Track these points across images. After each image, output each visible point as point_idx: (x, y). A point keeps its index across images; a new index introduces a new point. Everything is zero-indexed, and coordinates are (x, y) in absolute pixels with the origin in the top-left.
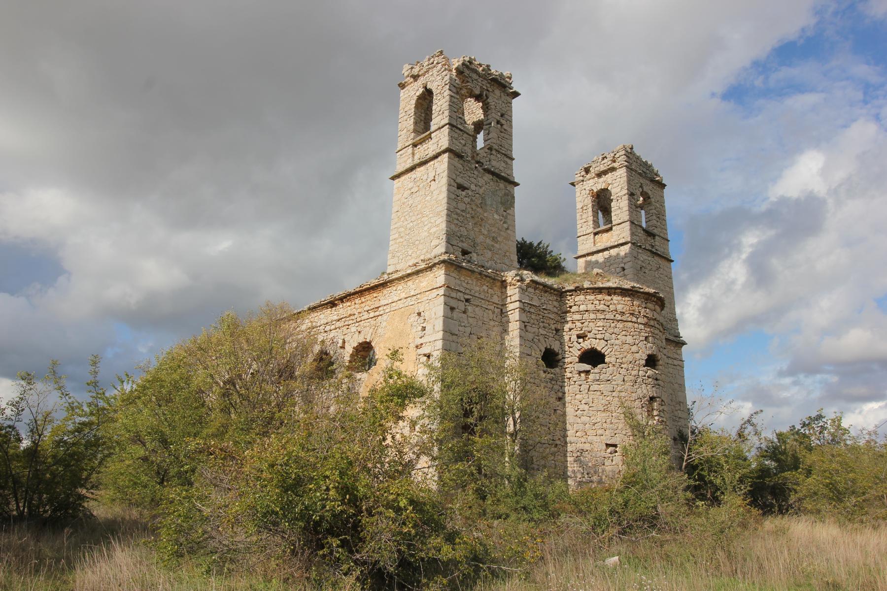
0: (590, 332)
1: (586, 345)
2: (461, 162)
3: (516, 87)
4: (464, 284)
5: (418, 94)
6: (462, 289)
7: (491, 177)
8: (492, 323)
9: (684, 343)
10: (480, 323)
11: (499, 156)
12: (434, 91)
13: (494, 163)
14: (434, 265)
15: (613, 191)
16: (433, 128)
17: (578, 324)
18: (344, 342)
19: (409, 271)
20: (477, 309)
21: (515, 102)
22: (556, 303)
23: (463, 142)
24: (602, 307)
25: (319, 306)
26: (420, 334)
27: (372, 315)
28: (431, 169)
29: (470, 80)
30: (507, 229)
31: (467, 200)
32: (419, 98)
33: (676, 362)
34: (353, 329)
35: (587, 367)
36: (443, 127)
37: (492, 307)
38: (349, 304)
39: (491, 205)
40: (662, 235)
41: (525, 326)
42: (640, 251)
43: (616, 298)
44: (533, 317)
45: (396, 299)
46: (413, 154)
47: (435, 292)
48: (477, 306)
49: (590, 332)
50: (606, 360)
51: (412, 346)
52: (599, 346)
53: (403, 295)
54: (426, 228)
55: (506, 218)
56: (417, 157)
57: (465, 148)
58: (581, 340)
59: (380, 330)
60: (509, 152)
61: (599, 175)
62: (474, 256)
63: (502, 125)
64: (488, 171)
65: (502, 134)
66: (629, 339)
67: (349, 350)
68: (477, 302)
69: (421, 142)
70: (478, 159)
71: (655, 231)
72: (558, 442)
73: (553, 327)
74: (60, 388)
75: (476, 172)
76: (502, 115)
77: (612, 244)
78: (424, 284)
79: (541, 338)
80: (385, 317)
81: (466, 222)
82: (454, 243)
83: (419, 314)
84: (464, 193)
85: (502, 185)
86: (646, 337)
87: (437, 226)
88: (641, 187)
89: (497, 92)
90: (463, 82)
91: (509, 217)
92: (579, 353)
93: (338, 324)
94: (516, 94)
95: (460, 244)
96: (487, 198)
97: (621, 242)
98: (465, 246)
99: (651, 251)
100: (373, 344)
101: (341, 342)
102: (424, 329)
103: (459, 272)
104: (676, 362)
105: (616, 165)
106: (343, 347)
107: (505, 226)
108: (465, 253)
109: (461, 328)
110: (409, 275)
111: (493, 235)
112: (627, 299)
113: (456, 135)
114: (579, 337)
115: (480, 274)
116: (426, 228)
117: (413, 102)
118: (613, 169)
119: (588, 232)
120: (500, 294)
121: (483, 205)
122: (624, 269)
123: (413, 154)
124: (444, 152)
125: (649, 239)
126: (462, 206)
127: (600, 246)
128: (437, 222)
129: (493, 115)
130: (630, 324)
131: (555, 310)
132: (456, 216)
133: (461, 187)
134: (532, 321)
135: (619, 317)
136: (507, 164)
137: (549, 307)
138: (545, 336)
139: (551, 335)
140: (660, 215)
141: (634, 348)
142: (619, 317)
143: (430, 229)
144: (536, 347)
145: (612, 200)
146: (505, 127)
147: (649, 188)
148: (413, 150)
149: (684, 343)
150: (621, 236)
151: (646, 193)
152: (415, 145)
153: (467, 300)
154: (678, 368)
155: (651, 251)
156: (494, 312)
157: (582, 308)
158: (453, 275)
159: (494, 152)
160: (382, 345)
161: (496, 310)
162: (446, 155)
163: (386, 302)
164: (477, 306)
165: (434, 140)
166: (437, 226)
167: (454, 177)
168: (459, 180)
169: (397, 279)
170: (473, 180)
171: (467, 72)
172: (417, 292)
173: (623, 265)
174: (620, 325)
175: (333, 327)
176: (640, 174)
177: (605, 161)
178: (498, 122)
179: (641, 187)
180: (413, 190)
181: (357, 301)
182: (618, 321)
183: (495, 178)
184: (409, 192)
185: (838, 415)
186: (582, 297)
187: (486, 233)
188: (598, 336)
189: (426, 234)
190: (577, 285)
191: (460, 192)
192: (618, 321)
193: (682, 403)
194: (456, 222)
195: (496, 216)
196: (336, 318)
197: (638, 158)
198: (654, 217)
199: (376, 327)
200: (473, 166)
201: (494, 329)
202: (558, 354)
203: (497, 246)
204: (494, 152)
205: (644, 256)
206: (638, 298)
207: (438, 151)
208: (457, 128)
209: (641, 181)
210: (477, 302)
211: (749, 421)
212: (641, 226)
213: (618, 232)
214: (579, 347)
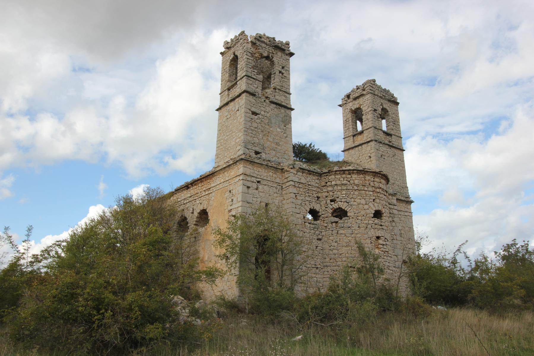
0: (338, 198)
1: (336, 206)
2: (254, 98)
3: (292, 49)
4: (257, 172)
5: (231, 58)
6: (255, 175)
7: (275, 106)
8: (275, 195)
9: (412, 202)
10: (268, 195)
11: (281, 93)
12: (238, 56)
13: (277, 97)
14: (237, 161)
15: (363, 109)
16: (238, 78)
17: (331, 193)
18: (193, 210)
19: (224, 166)
20: (265, 187)
21: (292, 59)
22: (317, 181)
23: (256, 86)
24: (345, 182)
25: (181, 188)
26: (231, 203)
27: (207, 193)
28: (237, 103)
29: (260, 48)
30: (286, 137)
31: (258, 121)
32: (231, 61)
33: (406, 214)
34: (198, 202)
35: (337, 219)
36: (243, 77)
37: (275, 185)
38: (195, 187)
39: (275, 123)
40: (396, 134)
41: (296, 196)
42: (381, 145)
43: (354, 176)
44: (301, 190)
45: (219, 183)
46: (228, 95)
47: (238, 178)
48: (265, 185)
49: (338, 198)
50: (348, 214)
51: (227, 210)
52: (344, 206)
53: (222, 181)
54: (234, 140)
55: (285, 130)
56: (230, 96)
57: (257, 89)
58: (333, 203)
59: (211, 202)
60: (287, 90)
61: (355, 99)
62: (263, 155)
63: (283, 74)
64: (272, 102)
65: (283, 79)
66: (363, 201)
67: (196, 214)
68: (265, 183)
69: (232, 86)
70: (267, 95)
71: (392, 132)
72: (319, 266)
73: (315, 196)
74: (11, 242)
75: (264, 104)
76: (283, 68)
77: (363, 142)
78: (232, 173)
79: (307, 203)
80: (213, 194)
81: (258, 134)
82: (250, 147)
83: (230, 191)
84: (256, 117)
85: (283, 110)
86: (374, 200)
87: (240, 138)
88: (382, 105)
89: (279, 54)
90: (256, 49)
91: (287, 129)
92: (331, 211)
93: (190, 199)
94: (292, 54)
95: (253, 148)
96: (272, 119)
97: (368, 140)
98: (257, 149)
99: (389, 145)
100: (207, 211)
101: (191, 209)
102: (232, 200)
103: (253, 165)
104: (406, 214)
105: (364, 92)
106: (193, 213)
107: (285, 135)
108: (257, 153)
109: (254, 199)
110: (225, 168)
111: (276, 141)
112: (361, 176)
113: (251, 82)
114: (331, 201)
115: (267, 165)
116: (234, 140)
117: (228, 63)
118: (362, 95)
119: (349, 135)
120: (281, 177)
121: (269, 123)
122: (370, 157)
123: (228, 95)
124: (243, 92)
125: (388, 137)
126: (255, 125)
127: (357, 143)
128: (240, 136)
129: (277, 68)
130: (364, 191)
131: (317, 185)
132: (251, 131)
133: (254, 113)
134: (300, 193)
135: (356, 188)
136: (286, 97)
137: (312, 183)
138: (310, 202)
139: (314, 200)
140: (395, 122)
141: (366, 207)
142: (356, 188)
143: (236, 140)
144: (303, 209)
145: (363, 115)
146: (284, 75)
147: (387, 105)
148: (228, 93)
149: (412, 202)
150: (369, 136)
151: (386, 109)
152: (229, 89)
153: (258, 182)
154: (408, 217)
155: (389, 145)
156: (276, 188)
157: (333, 183)
158: (249, 167)
159: (277, 91)
160: (211, 211)
161: (278, 187)
162: (244, 95)
163: (214, 185)
164: (265, 185)
165: (238, 86)
166: (240, 138)
167: (250, 107)
168: (253, 109)
169: (221, 170)
170: (262, 108)
171: (258, 43)
172: (230, 178)
173: (369, 155)
174: (356, 193)
175: (188, 201)
176: (381, 97)
177: (359, 90)
178: (280, 72)
179: (382, 105)
180: (228, 117)
181: (200, 185)
182: (355, 190)
183: (278, 107)
184: (226, 118)
185: (526, 242)
186: (333, 177)
187: (271, 140)
188: (343, 200)
189: (234, 143)
190: (329, 169)
191: (253, 116)
192: (355, 190)
193: (411, 238)
194: (251, 135)
195: (278, 130)
196: (189, 195)
197: (379, 87)
198: (391, 123)
199: (209, 200)
200: (263, 100)
201: (277, 198)
202: (319, 212)
203: (279, 148)
204: (277, 91)
205: (384, 148)
206: (369, 175)
207: (240, 92)
208: (251, 78)
209: (382, 101)
210: (265, 183)
211: (458, 250)
212: (381, 130)
213: (367, 134)
214: (331, 207)
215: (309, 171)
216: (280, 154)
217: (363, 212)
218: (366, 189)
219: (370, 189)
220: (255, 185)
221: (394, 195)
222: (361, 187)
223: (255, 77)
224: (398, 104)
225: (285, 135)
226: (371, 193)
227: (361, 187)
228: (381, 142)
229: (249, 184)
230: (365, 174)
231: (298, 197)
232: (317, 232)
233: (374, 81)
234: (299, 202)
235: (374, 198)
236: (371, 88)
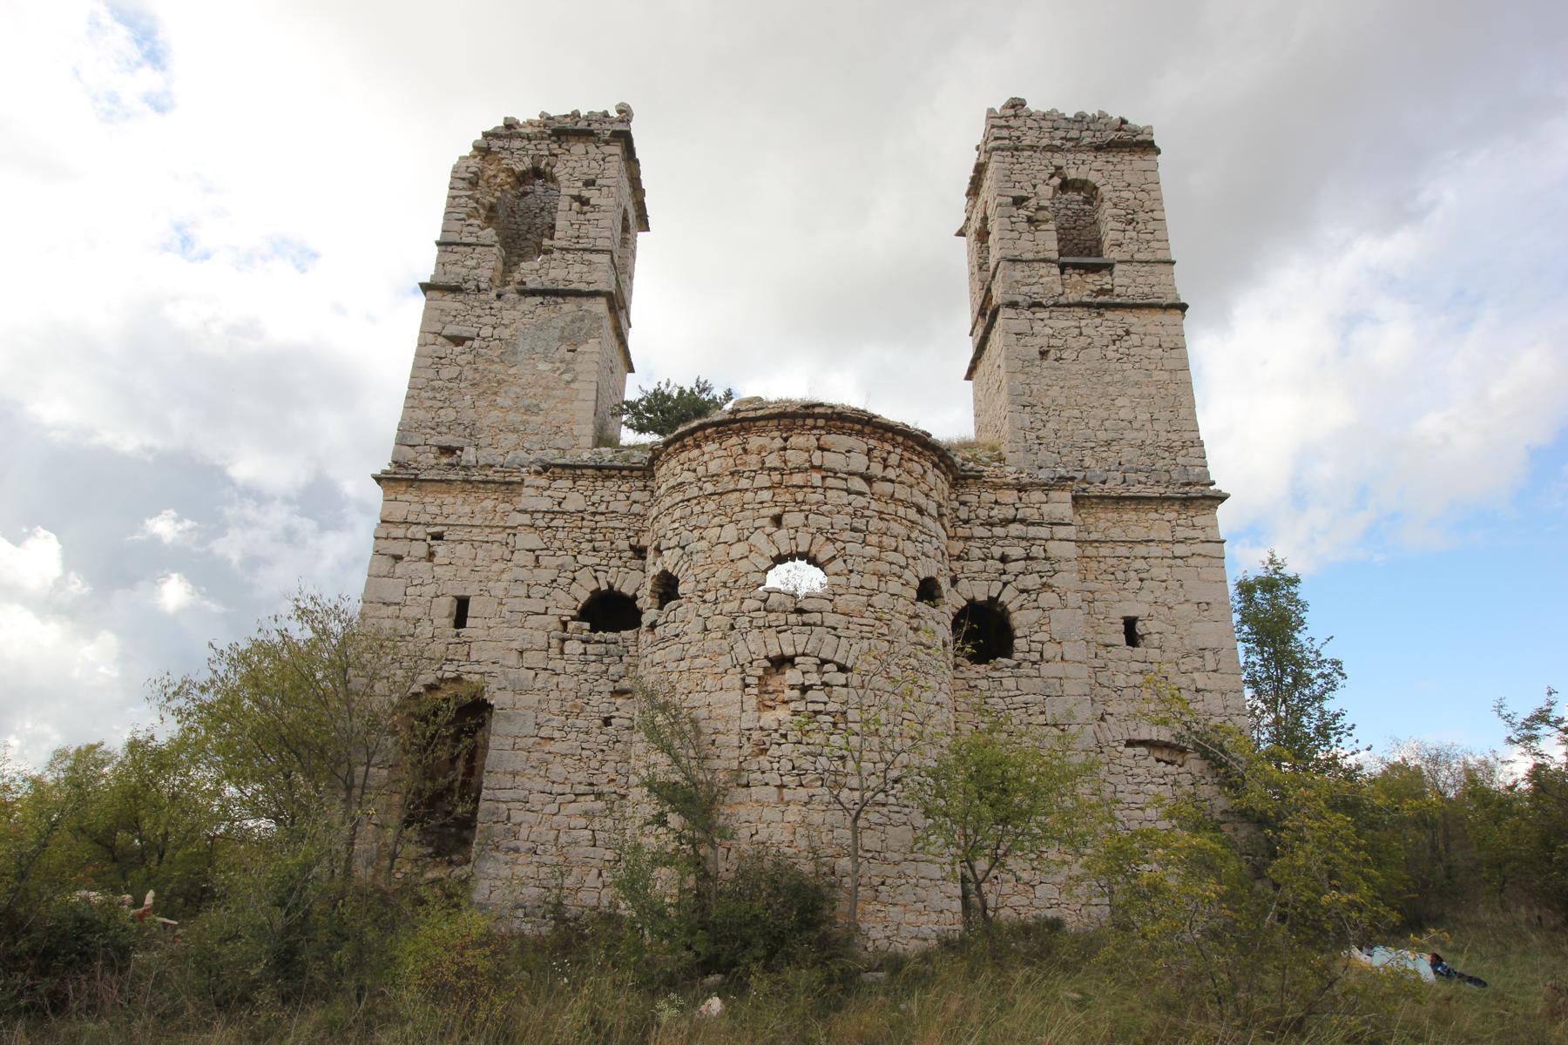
2: (461, 297)
9: (1222, 498)
11: (569, 256)
66: (730, 532)
68: (461, 534)
82: (418, 440)
98: (448, 440)
103: (419, 489)
107: (567, 377)
112: (734, 440)
132: (430, 394)
141: (739, 550)
142: (709, 488)
149: (1222, 498)
153: (438, 537)
158: (407, 497)
164: (461, 542)
167: (438, 327)
168: (452, 330)
174: (711, 506)
195: (542, 366)
206: (761, 432)
210: (461, 534)
215: (599, 468)
216: (534, 438)
217: (723, 574)
218: (744, 483)
219: (762, 480)
220: (420, 549)
221: (1061, 482)
222: (727, 483)
223: (472, 240)
224: (1147, 147)
225: (567, 377)
226: (766, 495)
227: (727, 483)
228: (1040, 305)
229: (397, 547)
230: (748, 431)
231: (544, 561)
232: (612, 669)
233: (1016, 105)
234: (545, 575)
235: (777, 510)
236: (622, 104)
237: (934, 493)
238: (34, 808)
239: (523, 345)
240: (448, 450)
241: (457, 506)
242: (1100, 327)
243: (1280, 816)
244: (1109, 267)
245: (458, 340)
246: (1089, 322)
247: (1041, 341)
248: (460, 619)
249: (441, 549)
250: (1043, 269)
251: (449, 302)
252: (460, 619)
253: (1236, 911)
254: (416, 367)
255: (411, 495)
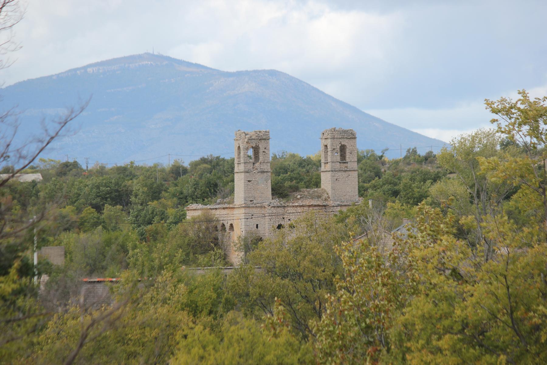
98: (251, 199)
168: (249, 179)
237: (242, 343)
238: (466, 161)
239: (260, 182)
240: (251, 201)
241: (255, 211)
242: (345, 174)
243: (187, 305)
244: (347, 163)
245: (249, 181)
246: (343, 173)
247: (336, 177)
248: (257, 227)
249: (253, 217)
250: (337, 163)
251: (248, 174)
252: (257, 227)
253: (433, 231)
254: (244, 187)
255: (248, 209)
